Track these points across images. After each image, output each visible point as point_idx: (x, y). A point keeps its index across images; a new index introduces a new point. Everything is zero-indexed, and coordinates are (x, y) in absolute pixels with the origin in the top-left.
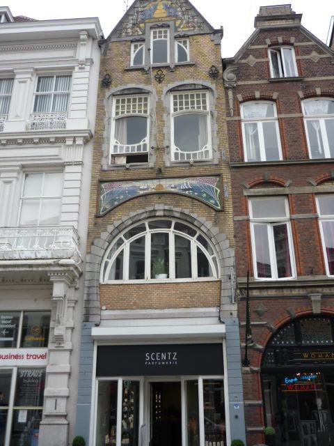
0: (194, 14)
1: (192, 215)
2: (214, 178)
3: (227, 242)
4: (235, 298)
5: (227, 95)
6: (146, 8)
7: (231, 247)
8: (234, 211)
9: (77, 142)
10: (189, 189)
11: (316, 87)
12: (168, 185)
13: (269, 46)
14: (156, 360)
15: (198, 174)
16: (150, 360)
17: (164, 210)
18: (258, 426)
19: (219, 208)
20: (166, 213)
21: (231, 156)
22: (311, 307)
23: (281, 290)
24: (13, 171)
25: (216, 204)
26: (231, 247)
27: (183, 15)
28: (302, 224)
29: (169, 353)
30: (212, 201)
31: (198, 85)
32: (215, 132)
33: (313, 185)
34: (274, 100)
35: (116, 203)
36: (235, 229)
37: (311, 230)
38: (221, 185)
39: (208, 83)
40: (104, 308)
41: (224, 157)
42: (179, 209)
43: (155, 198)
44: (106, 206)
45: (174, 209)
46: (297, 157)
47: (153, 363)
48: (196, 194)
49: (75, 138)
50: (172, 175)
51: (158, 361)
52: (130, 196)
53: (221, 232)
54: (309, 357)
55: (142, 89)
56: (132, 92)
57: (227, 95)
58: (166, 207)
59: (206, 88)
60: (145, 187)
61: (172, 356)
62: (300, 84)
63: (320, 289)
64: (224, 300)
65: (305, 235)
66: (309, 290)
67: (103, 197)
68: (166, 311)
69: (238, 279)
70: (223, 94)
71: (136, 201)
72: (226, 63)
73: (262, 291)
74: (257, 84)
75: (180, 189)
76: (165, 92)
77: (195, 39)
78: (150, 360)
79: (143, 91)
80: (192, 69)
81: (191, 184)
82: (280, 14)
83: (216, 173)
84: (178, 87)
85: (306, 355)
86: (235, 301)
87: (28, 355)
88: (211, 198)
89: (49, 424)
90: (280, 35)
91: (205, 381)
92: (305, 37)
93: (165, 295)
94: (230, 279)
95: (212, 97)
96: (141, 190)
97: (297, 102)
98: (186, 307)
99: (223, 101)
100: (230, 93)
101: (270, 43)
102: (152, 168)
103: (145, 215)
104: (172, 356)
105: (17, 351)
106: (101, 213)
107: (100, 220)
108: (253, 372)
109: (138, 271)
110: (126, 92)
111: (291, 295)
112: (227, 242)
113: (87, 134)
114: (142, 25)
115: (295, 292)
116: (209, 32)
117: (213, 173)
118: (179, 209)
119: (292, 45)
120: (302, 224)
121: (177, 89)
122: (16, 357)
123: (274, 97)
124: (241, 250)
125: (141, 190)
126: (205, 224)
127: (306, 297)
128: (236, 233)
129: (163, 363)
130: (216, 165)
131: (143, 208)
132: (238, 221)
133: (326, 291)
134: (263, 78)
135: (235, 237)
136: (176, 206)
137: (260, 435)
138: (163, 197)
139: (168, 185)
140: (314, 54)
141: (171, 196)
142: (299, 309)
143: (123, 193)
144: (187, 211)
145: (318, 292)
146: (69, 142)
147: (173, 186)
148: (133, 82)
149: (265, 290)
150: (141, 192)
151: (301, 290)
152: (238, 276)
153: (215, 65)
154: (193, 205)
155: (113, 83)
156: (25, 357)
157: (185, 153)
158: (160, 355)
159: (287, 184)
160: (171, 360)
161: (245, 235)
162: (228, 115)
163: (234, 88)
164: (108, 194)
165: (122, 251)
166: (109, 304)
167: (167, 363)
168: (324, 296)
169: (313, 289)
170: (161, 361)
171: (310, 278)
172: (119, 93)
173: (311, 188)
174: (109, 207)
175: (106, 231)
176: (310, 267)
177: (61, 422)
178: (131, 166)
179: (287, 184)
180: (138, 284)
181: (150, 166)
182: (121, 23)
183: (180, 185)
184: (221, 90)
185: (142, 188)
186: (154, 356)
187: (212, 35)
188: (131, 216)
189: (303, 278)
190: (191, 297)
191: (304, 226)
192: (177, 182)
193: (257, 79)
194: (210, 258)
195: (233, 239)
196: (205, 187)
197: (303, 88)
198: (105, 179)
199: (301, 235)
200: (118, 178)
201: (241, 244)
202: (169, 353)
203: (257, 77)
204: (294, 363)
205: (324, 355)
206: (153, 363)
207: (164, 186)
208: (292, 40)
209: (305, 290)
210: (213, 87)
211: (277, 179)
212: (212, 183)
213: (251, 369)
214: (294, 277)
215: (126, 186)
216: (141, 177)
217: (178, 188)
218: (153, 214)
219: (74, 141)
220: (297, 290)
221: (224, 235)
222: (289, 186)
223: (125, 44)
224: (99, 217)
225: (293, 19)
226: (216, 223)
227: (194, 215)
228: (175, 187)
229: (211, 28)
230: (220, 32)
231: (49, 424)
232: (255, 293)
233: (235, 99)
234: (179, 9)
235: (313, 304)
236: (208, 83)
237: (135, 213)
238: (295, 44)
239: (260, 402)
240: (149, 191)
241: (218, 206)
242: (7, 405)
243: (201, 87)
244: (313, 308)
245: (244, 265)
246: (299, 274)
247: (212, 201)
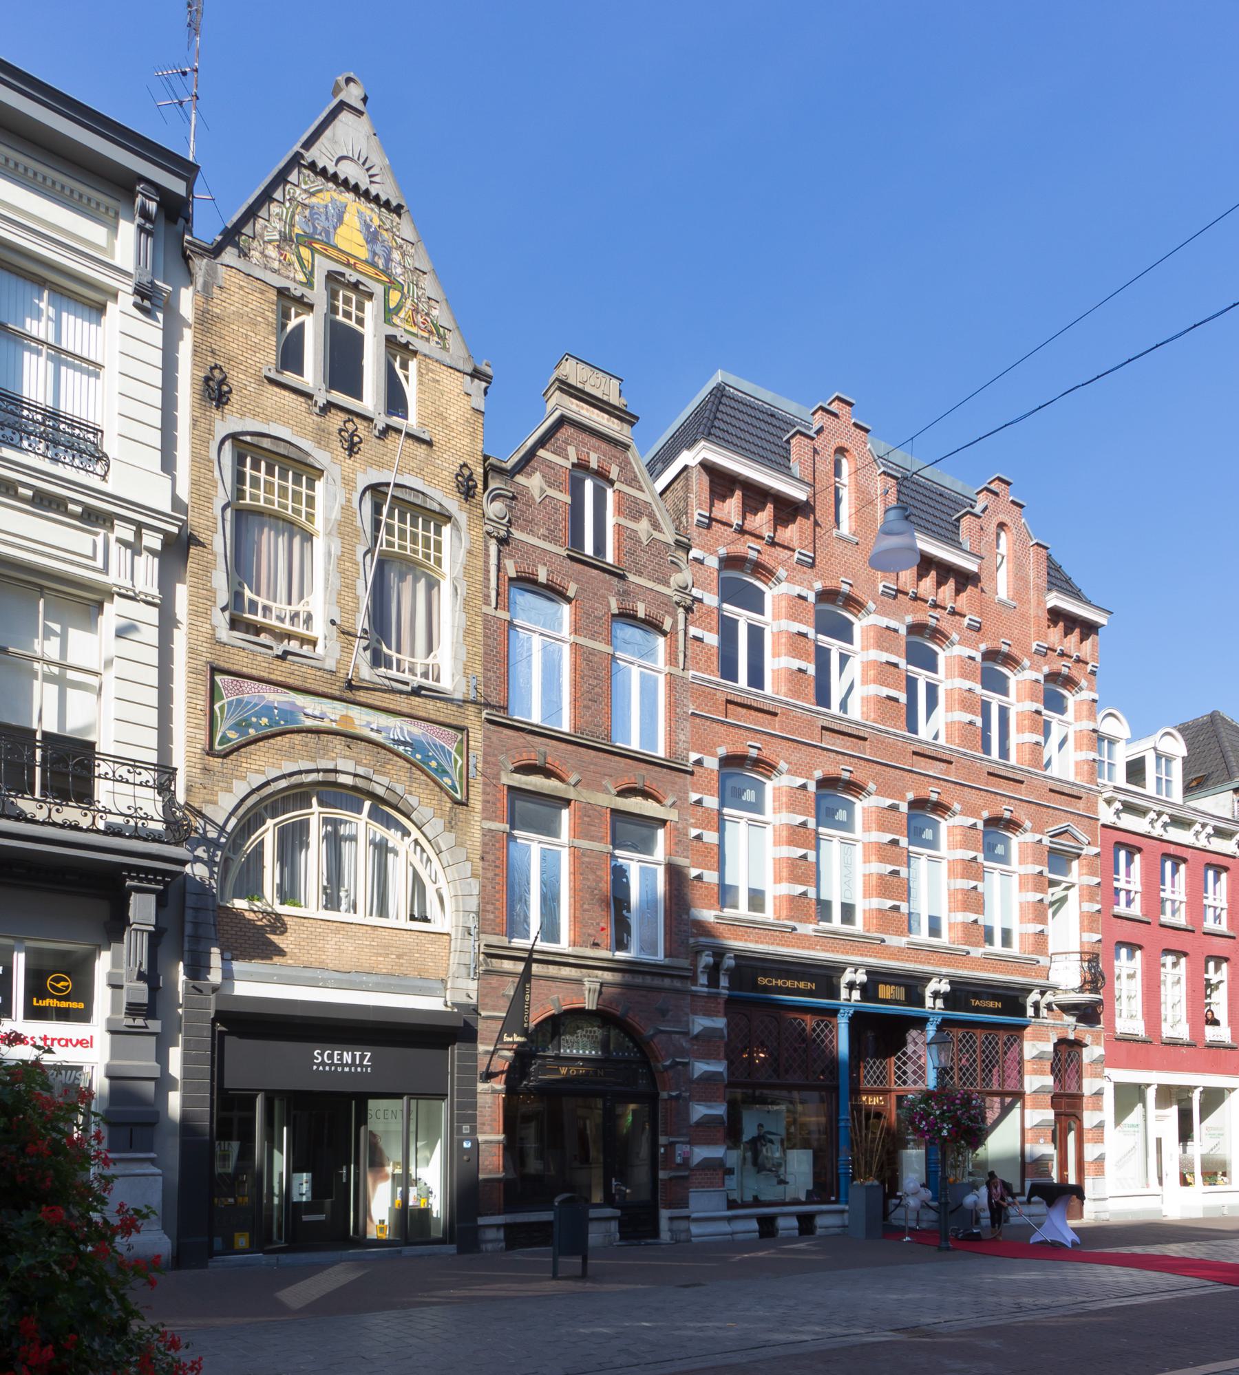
2: (452, 732)
7: (474, 876)
8: (484, 810)
10: (405, 743)
12: (363, 721)
14: (333, 1064)
17: (355, 775)
19: (459, 796)
23: (545, 966)
25: (454, 788)
26: (474, 876)
30: (447, 780)
31: (432, 499)
33: (609, 793)
36: (484, 844)
38: (465, 748)
39: (452, 504)
42: (384, 780)
43: (338, 742)
45: (375, 778)
46: (593, 733)
48: (418, 756)
49: (140, 526)
51: (337, 1065)
52: (283, 725)
53: (459, 844)
57: (487, 549)
58: (361, 771)
60: (317, 713)
61: (362, 1057)
63: (599, 973)
65: (588, 879)
66: (584, 971)
70: (480, 545)
77: (433, 371)
81: (409, 732)
88: (445, 772)
90: (596, 449)
91: (656, 955)
93: (349, 946)
95: (455, 539)
104: (362, 1057)
107: (215, 762)
108: (494, 1092)
111: (559, 976)
113: (175, 530)
115: (566, 972)
118: (384, 780)
123: (571, 593)
127: (579, 982)
128: (484, 852)
131: (313, 759)
132: (490, 830)
134: (1100, 1035)
135: (482, 859)
139: (363, 721)
144: (399, 789)
148: (286, 424)
150: (309, 723)
154: (412, 779)
155: (234, 397)
158: (341, 1055)
159: (573, 779)
160: (361, 1065)
164: (230, 703)
166: (236, 949)
167: (353, 1069)
170: (343, 1065)
177: (147, 1171)
179: (573, 779)
183: (387, 729)
184: (478, 532)
185: (309, 711)
186: (331, 1057)
190: (399, 957)
191: (590, 863)
193: (545, 538)
195: (480, 864)
196: (435, 745)
197: (618, 594)
200: (254, 673)
201: (490, 875)
202: (358, 1054)
207: (357, 722)
209: (578, 970)
211: (552, 762)
212: (446, 740)
214: (564, 945)
217: (384, 734)
218: (331, 777)
220: (568, 969)
223: (262, 292)
226: (451, 826)
227: (413, 800)
228: (378, 731)
232: (535, 956)
240: (326, 724)
243: (437, 508)
246: (574, 944)
247: (447, 780)
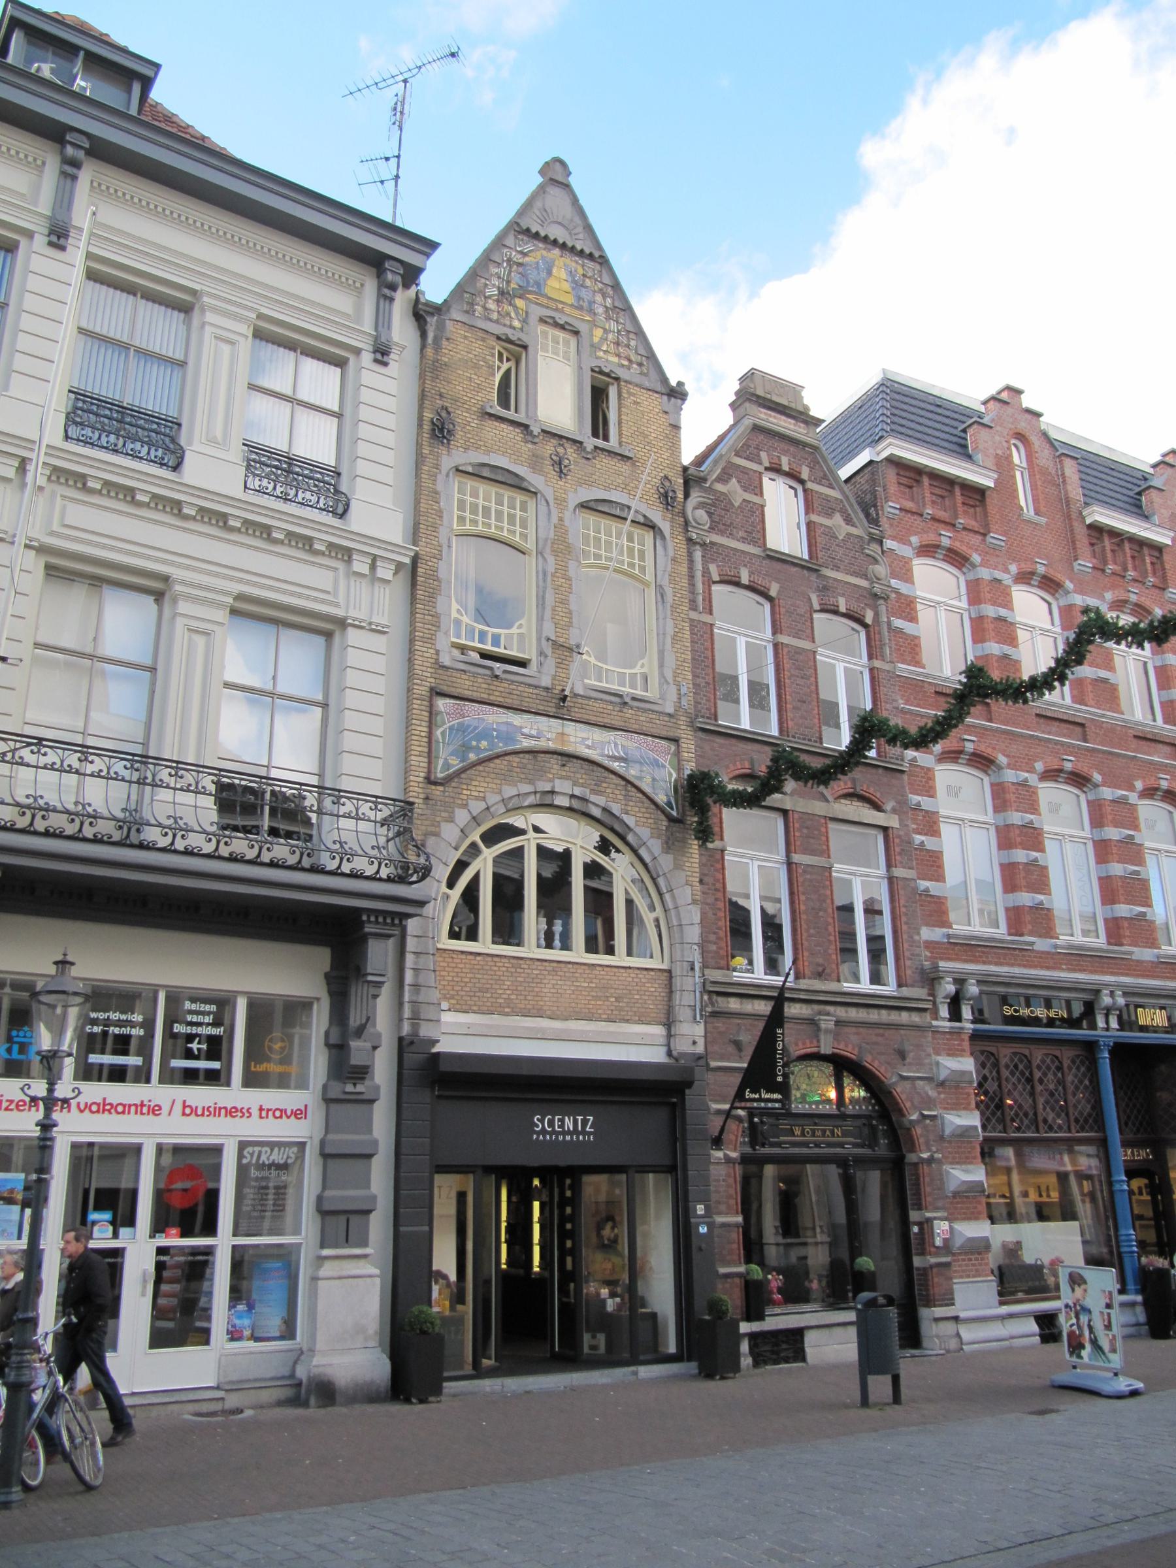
0: (630, 327)
1: (625, 817)
3: (688, 890)
4: (701, 1010)
5: (690, 555)
6: (527, 259)
7: (694, 902)
9: (381, 573)
11: (839, 594)
13: (767, 469)
15: (635, 727)
16: (544, 1131)
17: (572, 796)
18: (735, 1265)
19: (674, 813)
20: (576, 804)
21: (697, 703)
22: (818, 1041)
24: (218, 605)
26: (694, 902)
27: (608, 318)
28: (808, 877)
29: (580, 1118)
32: (669, 640)
34: (770, 599)
35: (472, 757)
37: (822, 891)
39: (657, 516)
40: (445, 1005)
41: (684, 702)
42: (601, 800)
43: (554, 763)
44: (447, 760)
45: (593, 798)
47: (548, 1137)
49: (375, 558)
50: (586, 717)
52: (501, 747)
54: (803, 1135)
55: (522, 479)
56: (500, 478)
57: (690, 555)
58: (577, 791)
59: (650, 526)
60: (534, 732)
61: (585, 1122)
62: (813, 577)
63: (831, 1009)
64: (683, 1013)
66: (816, 1007)
67: (443, 733)
68: (573, 1025)
69: (707, 971)
71: (515, 759)
72: (691, 479)
73: (744, 1001)
74: (743, 552)
75: (603, 755)
76: (571, 506)
77: (634, 395)
78: (544, 1131)
79: (525, 485)
80: (625, 468)
82: (785, 403)
83: (671, 734)
84: (597, 501)
85: (797, 1131)
86: (701, 1015)
87: (261, 1109)
89: (340, 1278)
92: (825, 477)
94: (692, 969)
96: (526, 736)
97: (808, 615)
98: (609, 1020)
99: (684, 569)
100: (698, 554)
101: (768, 465)
102: (546, 689)
103: (531, 800)
104: (585, 1122)
105: (235, 1094)
106: (440, 775)
107: (437, 791)
108: (728, 1160)
109: (507, 930)
110: (486, 473)
112: (688, 890)
114: (519, 303)
116: (659, 389)
117: (664, 733)
118: (601, 800)
119: (802, 482)
120: (808, 877)
121: (592, 504)
122: (231, 1112)
124: (710, 914)
125: (526, 736)
126: (649, 844)
127: (812, 1022)
129: (568, 1138)
130: (670, 715)
131: (531, 782)
133: (841, 1012)
134: (754, 542)
135: (701, 882)
136: (594, 792)
137: (737, 1280)
138: (570, 765)
140: (838, 519)
141: (586, 765)
142: (800, 1044)
143: (485, 735)
144: (616, 809)
145: (828, 1014)
146: (361, 565)
147: (589, 743)
149: (749, 1001)
150: (527, 744)
151: (804, 1006)
152: (705, 966)
153: (670, 474)
156: (255, 1112)
157: (491, 630)
158: (562, 1121)
160: (584, 1132)
161: (718, 881)
162: (693, 607)
163: (703, 545)
164: (451, 728)
165: (476, 879)
166: (452, 997)
168: (838, 1023)
169: (822, 1007)
170: (564, 1133)
171: (818, 985)
172: (470, 469)
173: (823, 804)
174: (456, 764)
175: (451, 820)
176: (818, 965)
178: (505, 672)
180: (514, 958)
181: (543, 684)
182: (474, 274)
185: (525, 731)
186: (551, 1123)
187: (665, 398)
188: (506, 796)
189: (906, 992)
190: (618, 999)
192: (598, 735)
193: (743, 540)
194: (648, 917)
197: (818, 590)
198: (445, 689)
199: (807, 899)
202: (580, 1118)
203: (744, 535)
204: (779, 1145)
205: (824, 1131)
206: (548, 1137)
208: (805, 474)
210: (665, 527)
213: (725, 1155)
214: (889, 988)
215: (495, 718)
216: (525, 705)
219: (373, 567)
220: (798, 1006)
221: (683, 874)
222: (792, 794)
223: (483, 340)
224: (435, 783)
225: (806, 422)
227: (630, 820)
229: (664, 380)
230: (677, 394)
231: (340, 1278)
233: (706, 572)
234: (599, 298)
235: (822, 1037)
236: (657, 516)
237: (514, 792)
238: (810, 485)
239: (402, 1229)
241: (672, 808)
242: (210, 1228)
244: (822, 1044)
245: (715, 943)
